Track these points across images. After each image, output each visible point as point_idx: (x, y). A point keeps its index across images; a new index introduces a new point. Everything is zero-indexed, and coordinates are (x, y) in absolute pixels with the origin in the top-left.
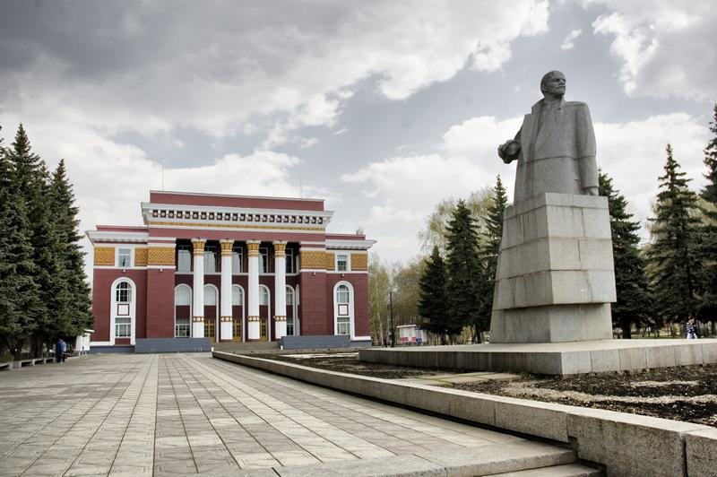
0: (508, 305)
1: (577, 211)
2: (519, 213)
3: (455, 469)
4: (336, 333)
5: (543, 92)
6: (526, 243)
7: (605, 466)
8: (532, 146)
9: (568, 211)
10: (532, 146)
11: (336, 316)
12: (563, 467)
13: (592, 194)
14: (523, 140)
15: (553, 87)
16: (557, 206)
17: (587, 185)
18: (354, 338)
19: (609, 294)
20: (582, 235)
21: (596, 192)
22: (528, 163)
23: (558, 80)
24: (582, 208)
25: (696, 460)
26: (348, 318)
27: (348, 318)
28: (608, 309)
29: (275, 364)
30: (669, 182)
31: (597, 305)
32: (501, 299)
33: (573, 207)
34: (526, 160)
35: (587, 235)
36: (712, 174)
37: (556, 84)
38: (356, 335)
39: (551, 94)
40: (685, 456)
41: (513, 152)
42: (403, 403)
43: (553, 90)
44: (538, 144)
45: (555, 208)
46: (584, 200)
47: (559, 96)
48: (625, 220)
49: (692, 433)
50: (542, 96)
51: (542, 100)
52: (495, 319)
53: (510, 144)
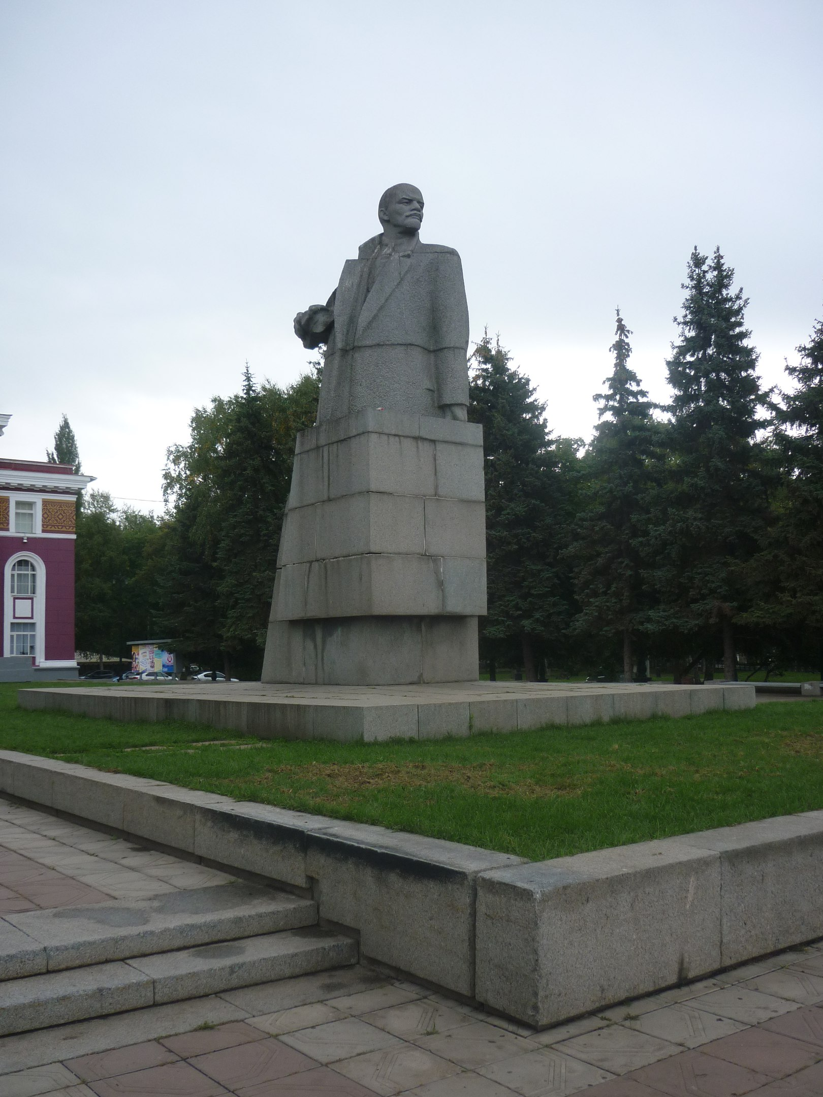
0: (297, 613)
1: (425, 448)
2: (322, 442)
3: (66, 948)
4: (7, 653)
5: (382, 221)
6: (329, 500)
7: (357, 932)
8: (352, 321)
9: (408, 444)
10: (352, 321)
11: (8, 619)
12: (283, 935)
13: (455, 418)
14: (337, 309)
15: (400, 214)
16: (389, 435)
17: (447, 400)
18: (42, 662)
19: (470, 592)
20: (432, 491)
21: (462, 414)
22: (345, 352)
23: (410, 201)
24: (433, 441)
25: (489, 922)
26: (33, 624)
27: (33, 624)
28: (474, 625)
29: (80, 697)
30: (616, 404)
31: (457, 620)
32: (286, 602)
33: (417, 439)
34: (340, 345)
35: (441, 491)
36: (677, 399)
37: (406, 209)
38: (48, 657)
39: (396, 226)
40: (473, 914)
41: (319, 329)
42: (48, 804)
43: (400, 220)
44: (363, 319)
45: (385, 437)
46: (439, 427)
47: (411, 232)
48: (55, 457)
49: (487, 875)
50: (380, 229)
51: (381, 235)
52: (274, 644)
53: (315, 311)
